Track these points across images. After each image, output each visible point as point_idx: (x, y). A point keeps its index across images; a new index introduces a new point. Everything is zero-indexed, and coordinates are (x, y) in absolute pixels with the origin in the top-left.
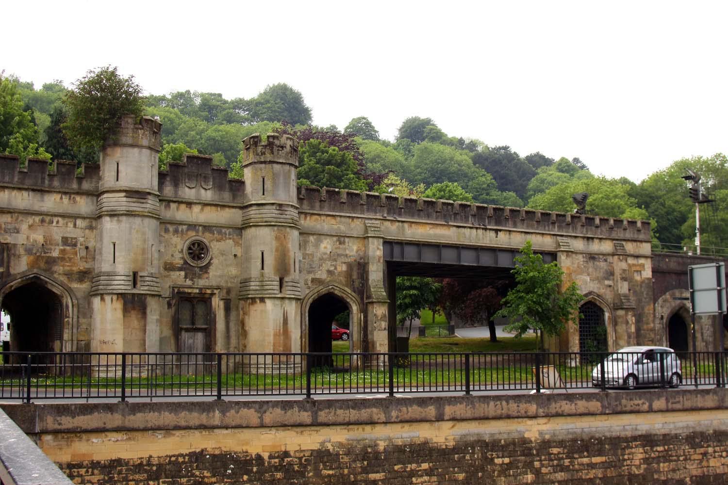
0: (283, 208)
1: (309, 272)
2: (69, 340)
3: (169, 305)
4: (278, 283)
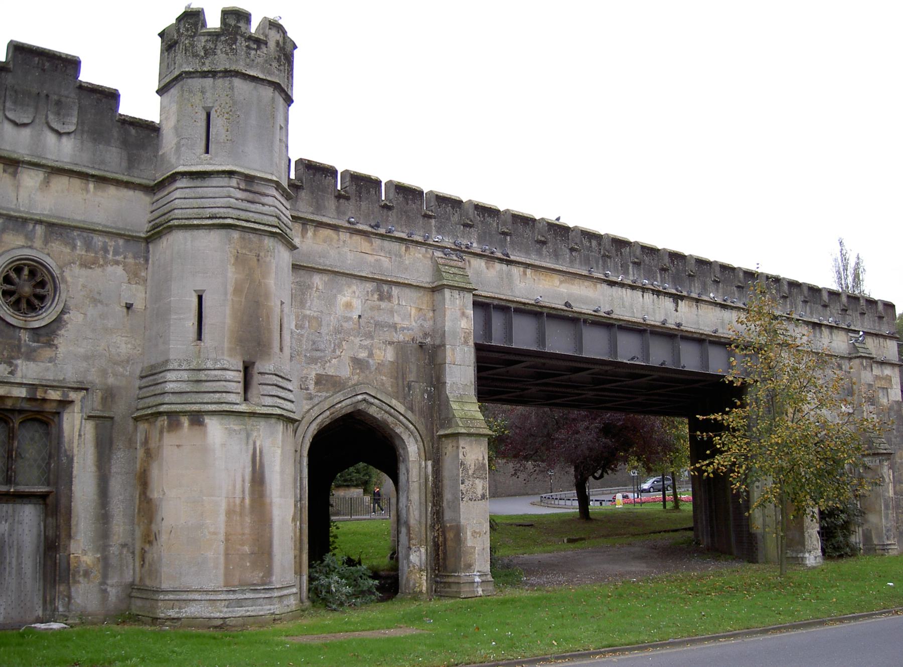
0: (256, 188)
1: (313, 361)
4: (240, 376)
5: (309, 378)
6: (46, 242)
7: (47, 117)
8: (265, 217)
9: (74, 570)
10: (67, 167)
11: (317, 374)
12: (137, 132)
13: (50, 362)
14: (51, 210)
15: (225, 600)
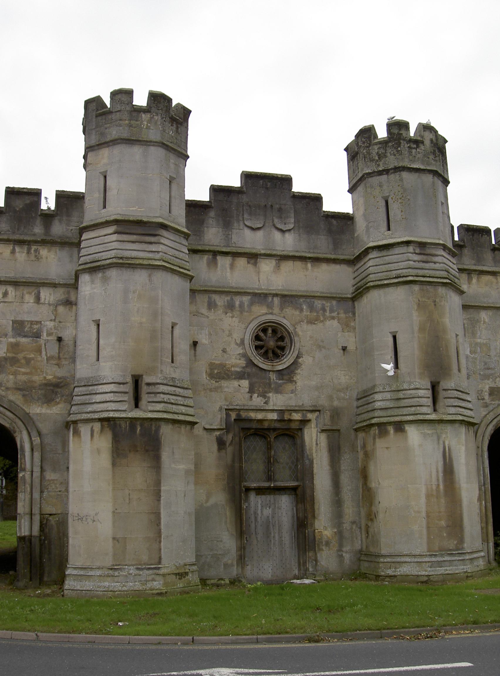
0: (428, 251)
1: (486, 377)
2: (25, 514)
3: (221, 443)
4: (429, 393)
5: (484, 391)
6: (282, 309)
7: (273, 221)
8: (438, 272)
9: (318, 541)
10: (291, 254)
11: (490, 387)
12: (337, 222)
13: (292, 393)
14: (283, 286)
15: (429, 562)
